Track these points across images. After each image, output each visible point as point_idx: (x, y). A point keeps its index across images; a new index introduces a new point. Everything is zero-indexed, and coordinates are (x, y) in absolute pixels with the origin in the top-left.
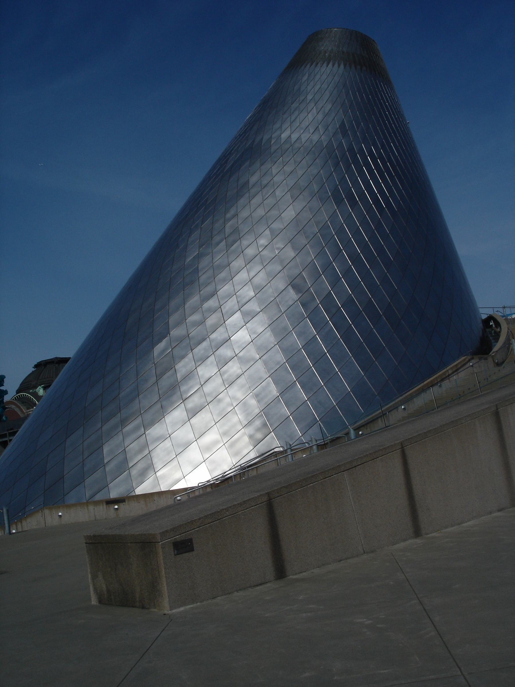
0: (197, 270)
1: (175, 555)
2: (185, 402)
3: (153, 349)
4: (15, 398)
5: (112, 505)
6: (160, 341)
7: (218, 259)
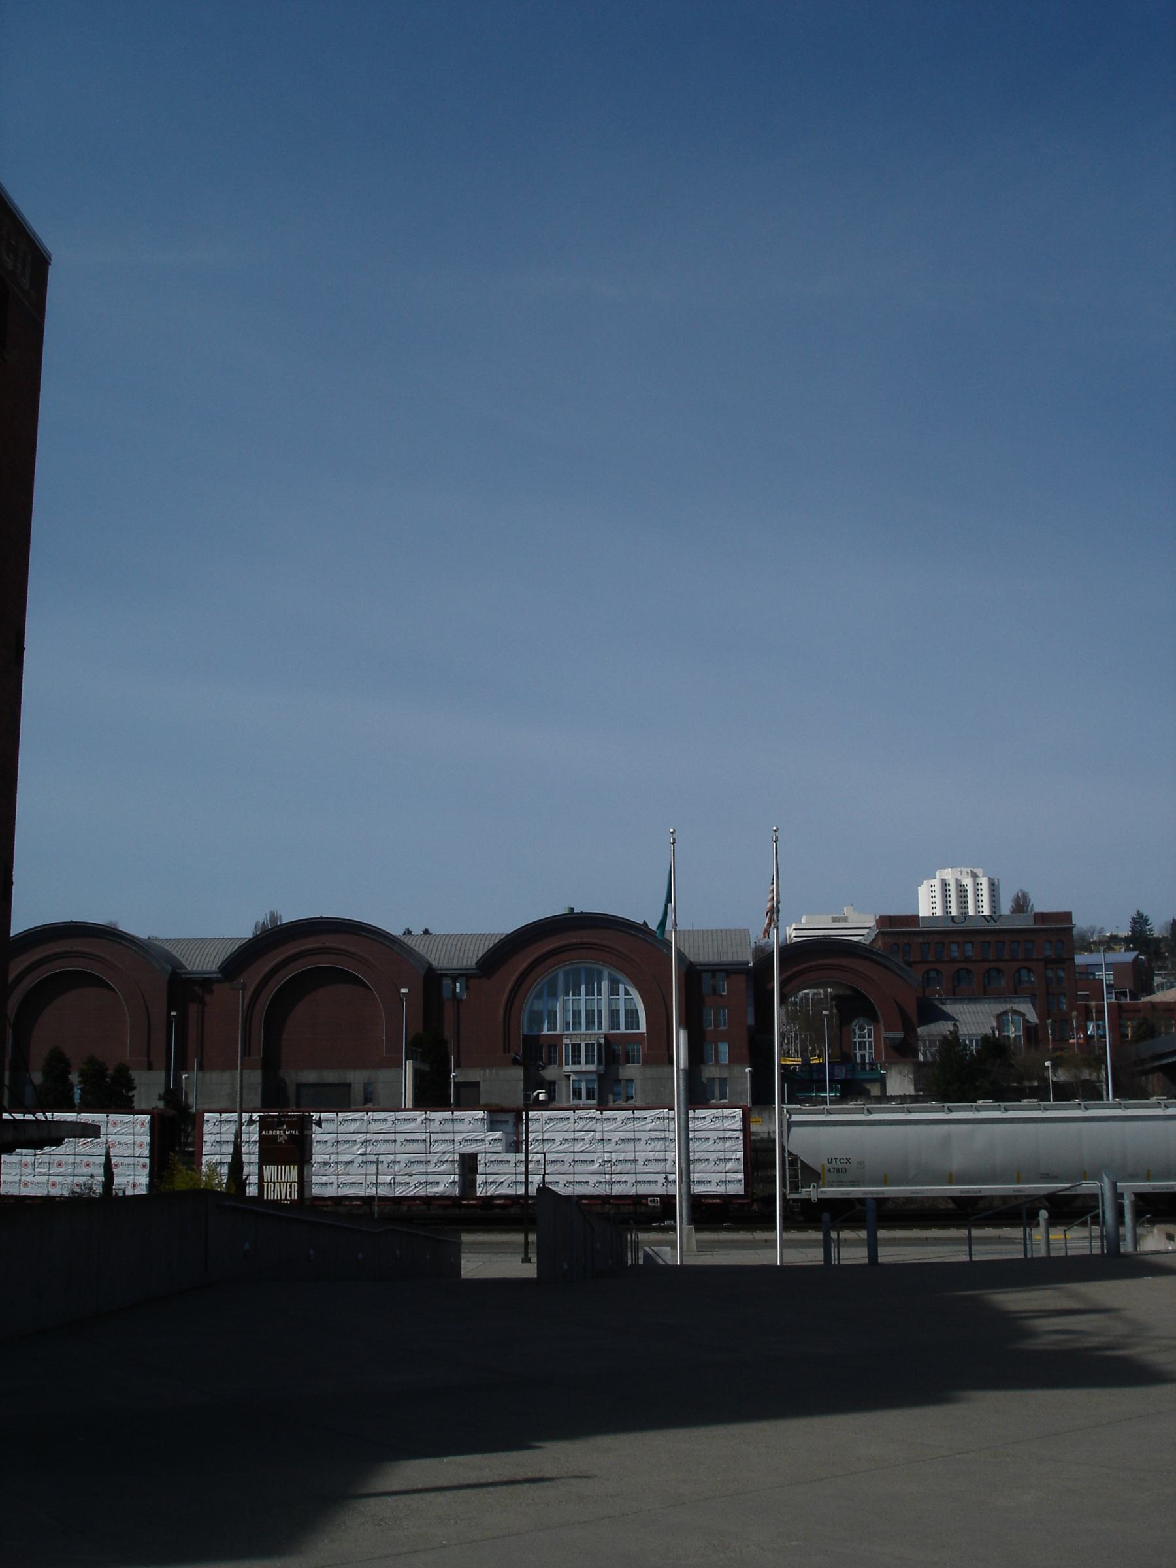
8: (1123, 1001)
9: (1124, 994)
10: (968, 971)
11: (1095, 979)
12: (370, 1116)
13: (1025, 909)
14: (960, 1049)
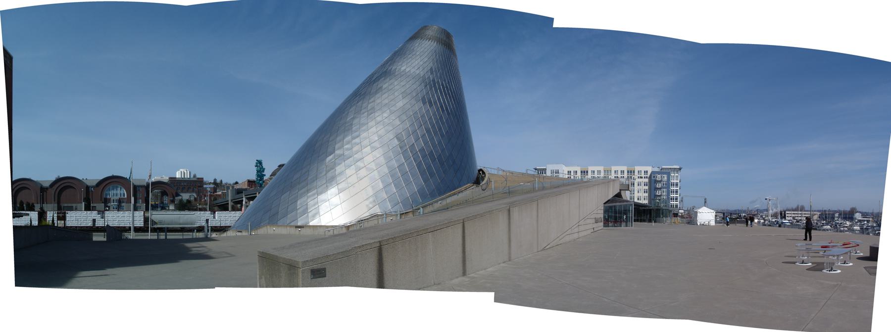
0: (352, 124)
6: (330, 155)
7: (363, 120)
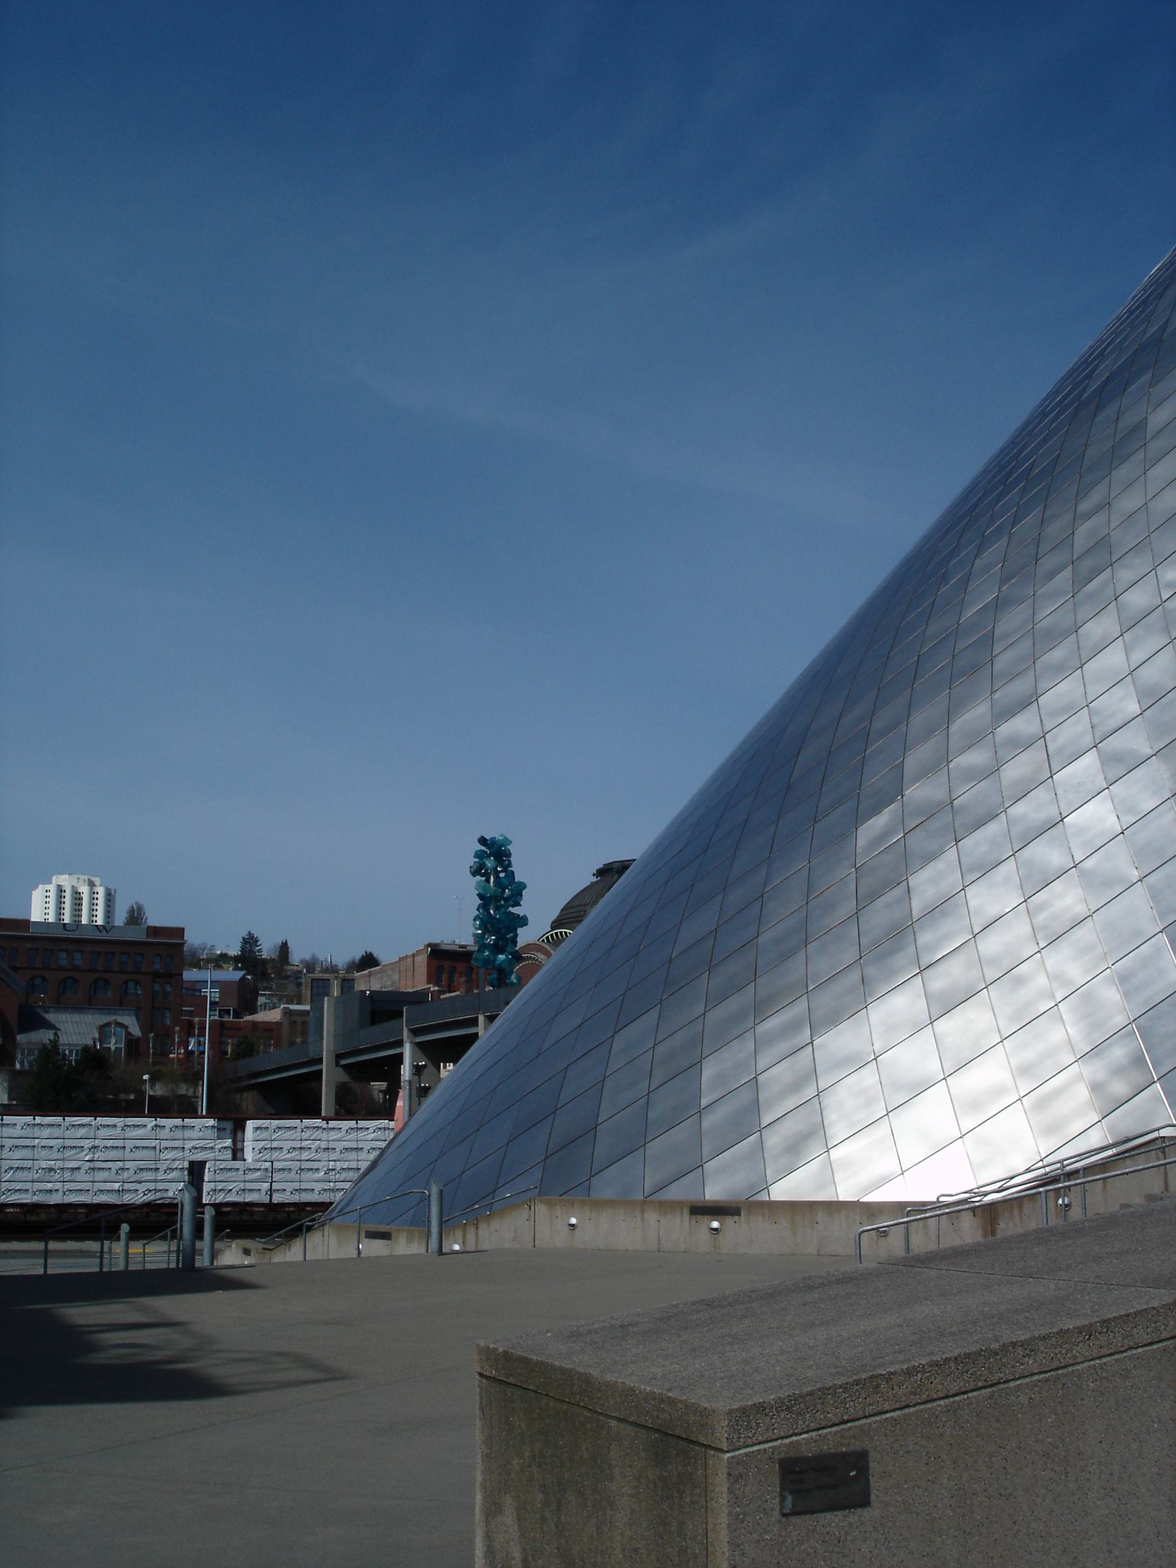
1: (784, 1515)
2: (926, 973)
3: (856, 830)
4: (547, 938)
5: (706, 1218)
6: (876, 810)
7: (1049, 614)
8: (226, 1019)
9: (228, 1012)
10: (75, 981)
11: (200, 995)
12: (98, 1122)
13: (139, 921)
14: (58, 1059)
